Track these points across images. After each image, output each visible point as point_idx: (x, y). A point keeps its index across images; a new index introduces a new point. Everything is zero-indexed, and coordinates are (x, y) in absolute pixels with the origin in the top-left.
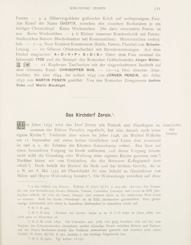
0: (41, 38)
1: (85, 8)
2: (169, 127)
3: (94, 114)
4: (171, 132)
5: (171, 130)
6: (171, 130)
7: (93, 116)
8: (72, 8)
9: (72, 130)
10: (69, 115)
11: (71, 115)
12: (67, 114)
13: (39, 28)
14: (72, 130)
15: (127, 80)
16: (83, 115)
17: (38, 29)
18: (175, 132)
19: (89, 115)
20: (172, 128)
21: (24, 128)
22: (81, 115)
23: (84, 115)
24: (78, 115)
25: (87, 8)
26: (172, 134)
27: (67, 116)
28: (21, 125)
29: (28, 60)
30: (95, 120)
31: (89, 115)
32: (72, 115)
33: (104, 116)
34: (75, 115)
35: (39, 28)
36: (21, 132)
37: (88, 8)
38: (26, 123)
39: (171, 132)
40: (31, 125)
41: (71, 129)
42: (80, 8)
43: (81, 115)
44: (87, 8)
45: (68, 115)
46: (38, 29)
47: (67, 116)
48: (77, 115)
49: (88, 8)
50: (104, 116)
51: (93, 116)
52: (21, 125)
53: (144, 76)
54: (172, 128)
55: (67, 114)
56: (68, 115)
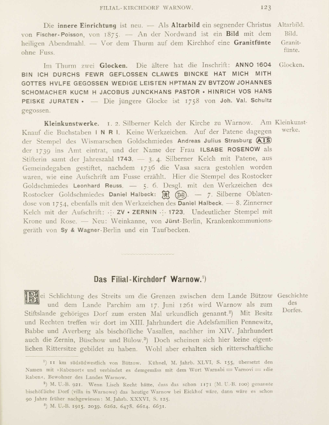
0: (125, 339)
1: (149, 8)
2: (288, 300)
3: (164, 278)
4: (292, 307)
5: (290, 303)
6: (290, 303)
7: (162, 280)
8: (127, 8)
9: (111, 305)
10: (99, 280)
11: (103, 280)
12: (96, 278)
13: (260, 24)
14: (111, 305)
15: (247, 203)
16: (145, 280)
17: (257, 25)
18: (297, 307)
19: (155, 280)
20: (293, 300)
21: (37, 302)
22: (142, 280)
23: (147, 280)
24: (137, 279)
25: (153, 8)
26: (293, 311)
27: (96, 280)
28: (32, 297)
29: (104, 160)
30: (167, 287)
31: (155, 280)
32: (105, 280)
33: (185, 280)
34: (109, 279)
35: (260, 24)
36: (32, 308)
37: (155, 8)
38: (41, 293)
39: (292, 307)
40: (47, 296)
41: (109, 304)
42: (140, 9)
43: (142, 280)
44: (153, 8)
45: (98, 279)
46: (257, 25)
47: (96, 280)
48: (134, 279)
49: (155, 8)
50: (185, 280)
51: (162, 280)
52: (32, 297)
53: (60, 213)
54: (293, 300)
55: (96, 278)
56: (98, 279)
